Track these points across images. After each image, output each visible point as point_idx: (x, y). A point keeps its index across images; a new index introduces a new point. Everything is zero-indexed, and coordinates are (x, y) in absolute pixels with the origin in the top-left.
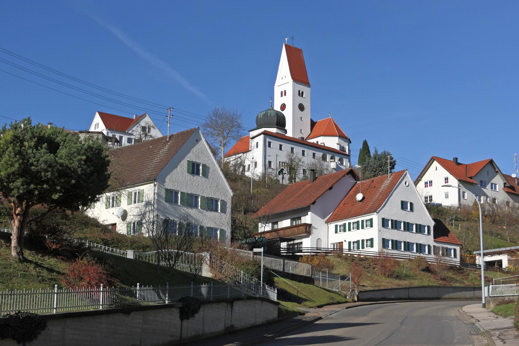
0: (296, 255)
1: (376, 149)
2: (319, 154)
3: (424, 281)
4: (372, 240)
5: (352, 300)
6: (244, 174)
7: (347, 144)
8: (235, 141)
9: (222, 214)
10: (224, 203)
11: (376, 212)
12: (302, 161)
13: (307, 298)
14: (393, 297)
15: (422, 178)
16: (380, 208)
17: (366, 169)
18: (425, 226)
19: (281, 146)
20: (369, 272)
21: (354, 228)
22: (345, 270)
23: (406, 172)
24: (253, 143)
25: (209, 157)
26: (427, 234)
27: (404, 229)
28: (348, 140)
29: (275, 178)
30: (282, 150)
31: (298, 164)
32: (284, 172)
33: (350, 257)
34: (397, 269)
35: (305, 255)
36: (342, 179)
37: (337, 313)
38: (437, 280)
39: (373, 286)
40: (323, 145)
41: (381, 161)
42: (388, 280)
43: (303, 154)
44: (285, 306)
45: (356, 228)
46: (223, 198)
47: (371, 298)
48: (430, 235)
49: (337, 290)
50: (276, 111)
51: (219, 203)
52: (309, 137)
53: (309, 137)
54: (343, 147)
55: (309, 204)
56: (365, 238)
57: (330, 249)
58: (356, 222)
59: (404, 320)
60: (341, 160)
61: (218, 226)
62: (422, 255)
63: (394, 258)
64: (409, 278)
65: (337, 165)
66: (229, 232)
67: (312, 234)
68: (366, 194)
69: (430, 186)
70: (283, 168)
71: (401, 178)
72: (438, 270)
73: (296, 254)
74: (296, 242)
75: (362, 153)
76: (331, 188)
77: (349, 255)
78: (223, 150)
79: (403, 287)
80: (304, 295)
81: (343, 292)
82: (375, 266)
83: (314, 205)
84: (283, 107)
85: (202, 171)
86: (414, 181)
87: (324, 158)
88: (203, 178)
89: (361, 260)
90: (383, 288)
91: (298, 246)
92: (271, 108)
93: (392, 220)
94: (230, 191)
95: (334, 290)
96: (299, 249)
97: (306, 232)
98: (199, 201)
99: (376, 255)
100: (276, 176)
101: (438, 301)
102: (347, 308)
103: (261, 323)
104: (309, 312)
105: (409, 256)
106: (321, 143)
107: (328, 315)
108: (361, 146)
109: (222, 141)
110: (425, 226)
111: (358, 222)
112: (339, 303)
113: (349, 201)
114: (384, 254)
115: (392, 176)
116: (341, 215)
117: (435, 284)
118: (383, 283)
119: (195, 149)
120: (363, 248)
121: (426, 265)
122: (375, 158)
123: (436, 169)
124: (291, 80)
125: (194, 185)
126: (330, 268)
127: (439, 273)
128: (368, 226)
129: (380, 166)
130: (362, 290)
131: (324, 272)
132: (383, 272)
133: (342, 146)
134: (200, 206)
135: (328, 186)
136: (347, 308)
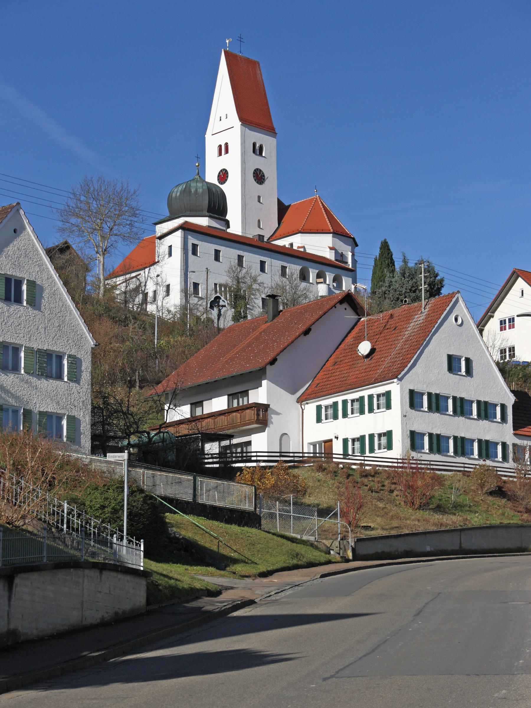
0: (232, 467)
1: (405, 257)
2: (294, 268)
3: (492, 515)
4: (389, 434)
5: (342, 557)
6: (146, 309)
7: (350, 248)
8: (126, 243)
9: (71, 384)
10: (75, 362)
11: (397, 377)
12: (259, 282)
13: (241, 557)
14: (428, 549)
15: (494, 312)
16: (406, 369)
17: (386, 295)
18: (496, 405)
19: (217, 253)
20: (380, 500)
21: (355, 411)
22: (331, 496)
23: (456, 296)
24: (162, 248)
25: (41, 265)
26: (499, 421)
27: (455, 411)
28: (352, 240)
29: (205, 316)
30: (219, 261)
31: (250, 287)
32: (221, 303)
33: (342, 469)
34: (437, 492)
35: (247, 467)
36: (329, 312)
37: (296, 588)
38: (518, 512)
39: (387, 527)
40: (302, 250)
41: (414, 280)
42: (420, 514)
43: (262, 269)
44: (170, 578)
45: (358, 411)
46: (73, 351)
47: (383, 552)
48: (506, 423)
49: (312, 538)
50: (208, 183)
51: (65, 362)
52: (275, 236)
53: (275, 236)
54: (342, 255)
55: (263, 364)
56: (377, 431)
57: (306, 455)
58: (357, 400)
59: (427, 604)
60: (337, 280)
61: (63, 409)
62: (489, 463)
63: (433, 469)
64: (462, 511)
65: (329, 289)
66: (87, 421)
67: (271, 426)
68: (377, 343)
69: (510, 328)
70: (218, 295)
71: (448, 309)
72: (520, 493)
73: (234, 465)
74: (235, 441)
75: (379, 266)
76: (307, 332)
77: (341, 466)
78: (102, 263)
79: (448, 528)
80: (235, 551)
81: (324, 541)
82: (393, 486)
83: (273, 366)
84: (223, 176)
85: (27, 296)
86: (478, 319)
87: (304, 276)
88: (30, 309)
89: (366, 476)
90: (407, 532)
91: (242, 449)
92: (197, 177)
93: (430, 395)
94: (89, 337)
95: (305, 538)
96: (244, 455)
97: (258, 421)
98: (21, 358)
99: (396, 465)
100: (206, 311)
101: (521, 555)
102: (323, 576)
103: (99, 621)
104: (232, 588)
105: (462, 465)
106: (299, 247)
107: (273, 593)
108: (377, 252)
109: (99, 244)
110: (496, 405)
111: (362, 399)
112: (311, 565)
113: (343, 357)
114: (411, 462)
115: (430, 305)
116: (328, 386)
117: (515, 522)
118: (408, 522)
119: (10, 249)
120: (372, 450)
121: (497, 483)
122: (403, 275)
123: (522, 295)
124: (237, 123)
125: (10, 323)
126: (298, 492)
127: (523, 499)
128: (381, 406)
129: (413, 289)
130: (363, 536)
131: (286, 502)
132: (409, 498)
133: (340, 252)
134: (25, 368)
135: (302, 328)
136: (323, 576)
